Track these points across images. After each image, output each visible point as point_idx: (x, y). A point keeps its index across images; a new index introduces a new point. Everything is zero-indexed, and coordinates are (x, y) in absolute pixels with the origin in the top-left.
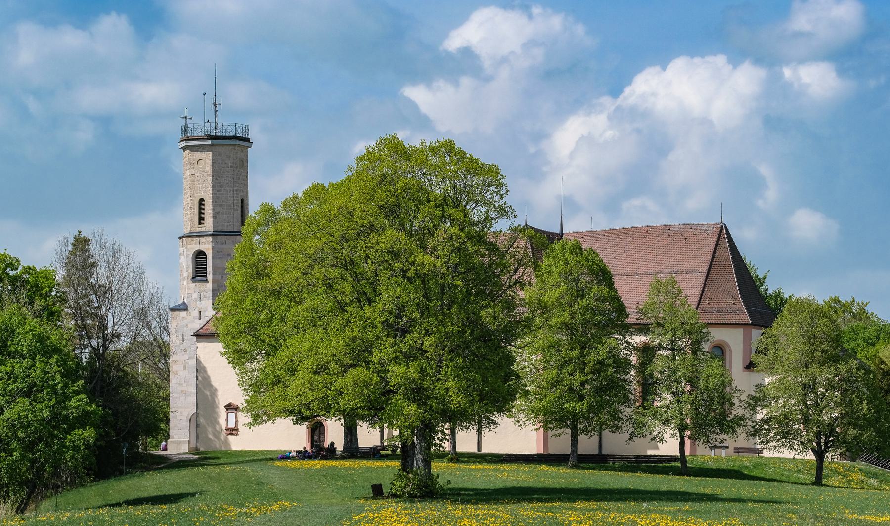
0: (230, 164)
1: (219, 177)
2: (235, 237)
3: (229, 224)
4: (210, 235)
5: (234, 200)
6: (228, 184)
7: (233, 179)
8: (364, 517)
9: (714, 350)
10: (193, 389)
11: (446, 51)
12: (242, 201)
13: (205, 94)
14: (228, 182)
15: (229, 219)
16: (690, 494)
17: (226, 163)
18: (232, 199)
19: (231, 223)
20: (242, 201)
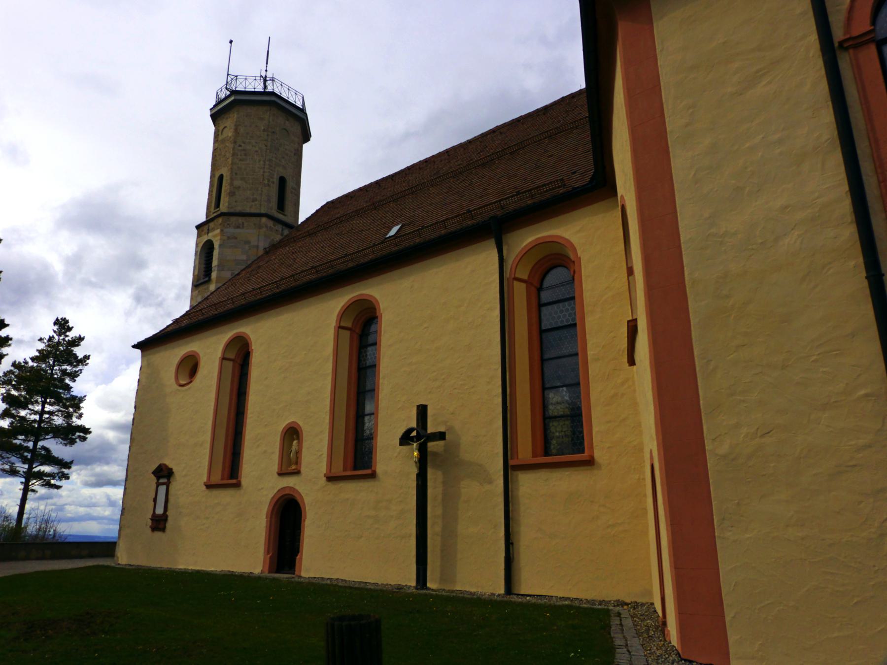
0: (262, 128)
1: (244, 143)
2: (258, 219)
3: (253, 203)
4: (555, 417)
5: (264, 172)
6: (257, 151)
7: (266, 146)
8: (8, 458)
9: (554, 451)
10: (178, 297)
11: (31, 536)
12: (282, 181)
13: (231, 42)
14: (257, 149)
15: (255, 197)
16: (503, 262)
17: (257, 126)
18: (262, 171)
19: (256, 203)
20: (282, 181)
